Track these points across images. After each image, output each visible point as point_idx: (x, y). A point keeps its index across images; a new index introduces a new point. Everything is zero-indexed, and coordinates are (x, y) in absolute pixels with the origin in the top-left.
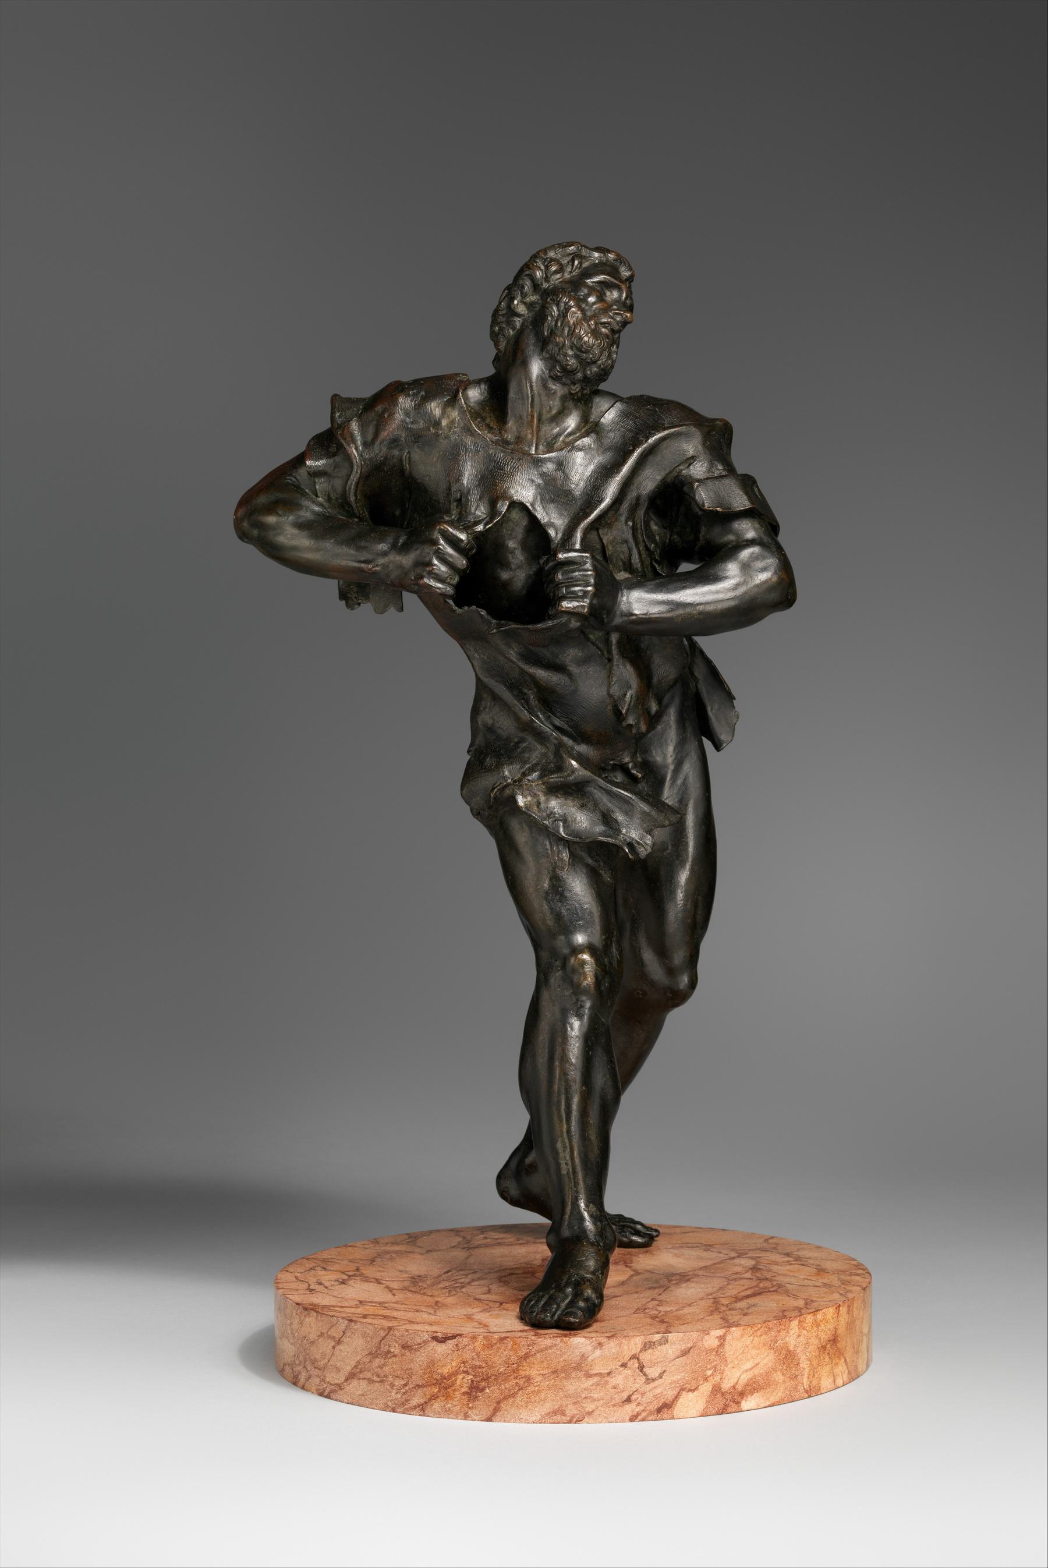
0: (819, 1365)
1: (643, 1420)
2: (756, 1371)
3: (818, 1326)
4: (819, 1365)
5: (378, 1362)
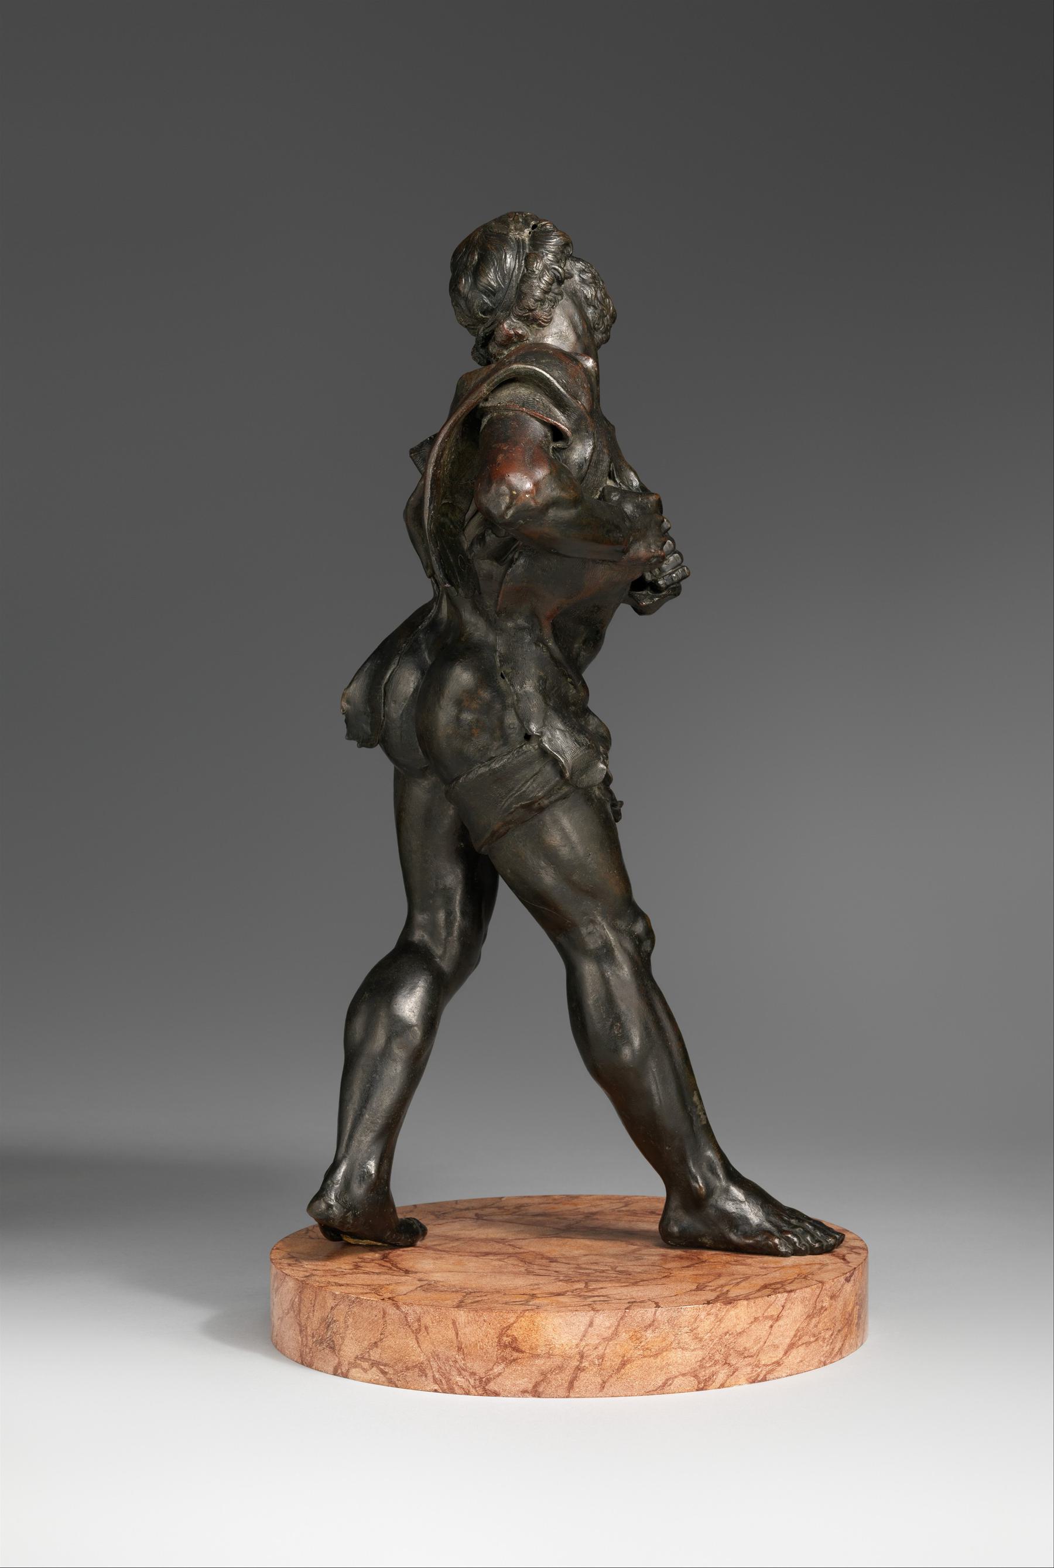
1: (722, 1386)
5: (814, 1321)
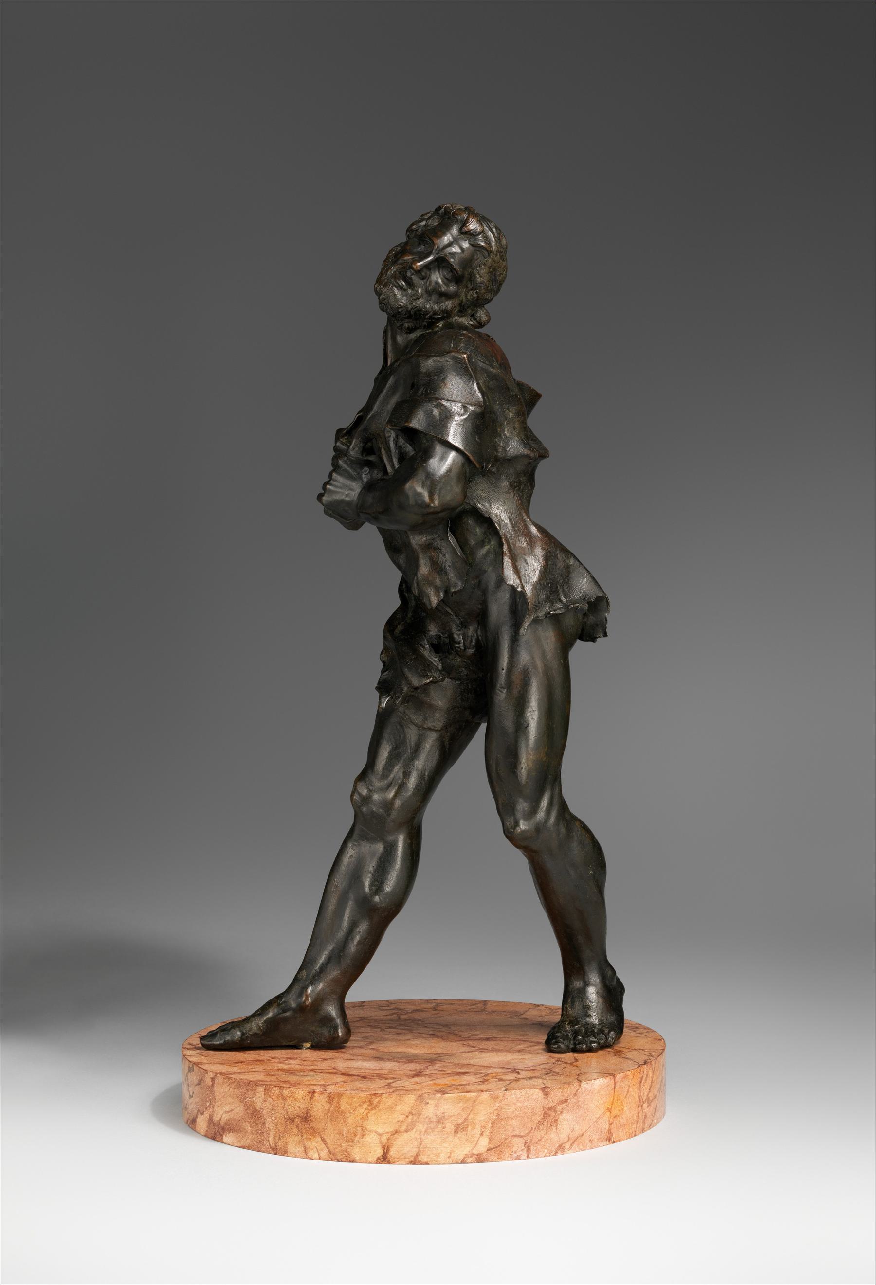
0: (285, 1132)
2: (232, 1115)
3: (284, 1099)
4: (285, 1132)
